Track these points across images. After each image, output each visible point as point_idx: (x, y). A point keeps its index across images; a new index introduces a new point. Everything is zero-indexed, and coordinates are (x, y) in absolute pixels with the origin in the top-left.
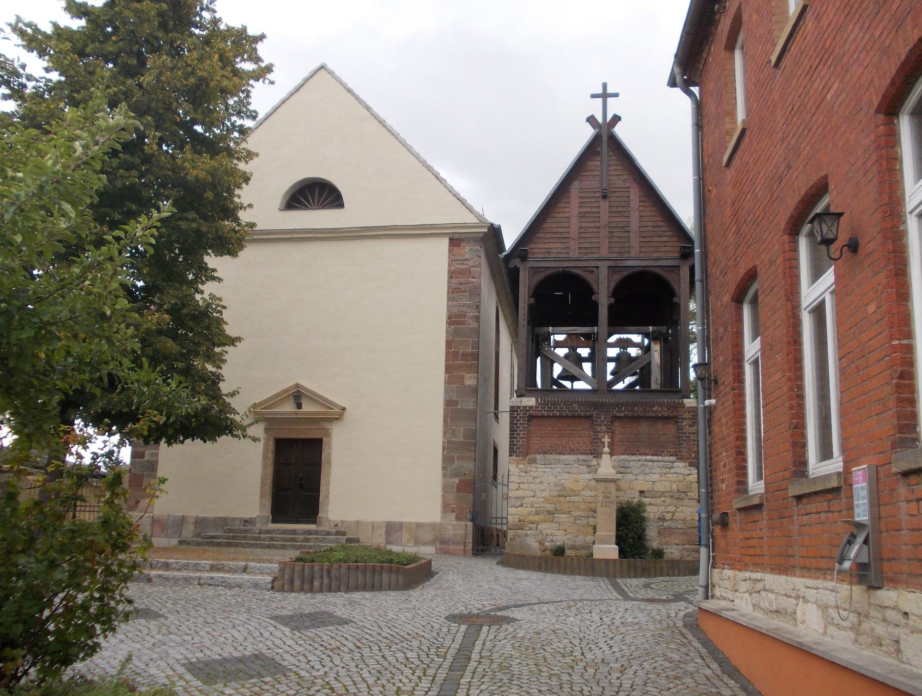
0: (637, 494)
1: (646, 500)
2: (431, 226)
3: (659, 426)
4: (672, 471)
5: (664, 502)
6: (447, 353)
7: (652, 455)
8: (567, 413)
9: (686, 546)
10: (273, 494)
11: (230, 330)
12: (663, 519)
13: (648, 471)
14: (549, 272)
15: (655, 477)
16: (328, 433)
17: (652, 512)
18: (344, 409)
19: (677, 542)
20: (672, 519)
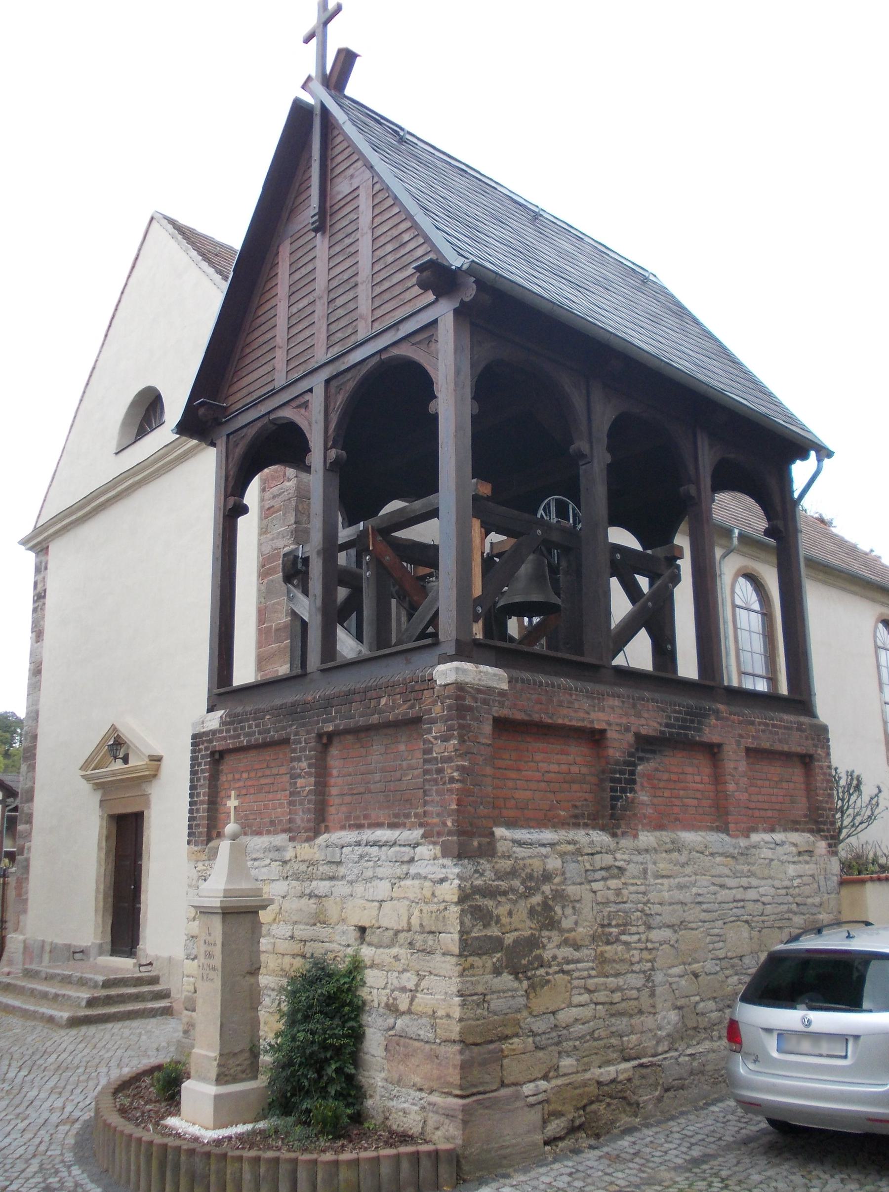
0: (353, 935)
1: (367, 953)
2: (271, 399)
3: (402, 747)
4: (413, 870)
5: (396, 958)
6: (260, 632)
7: (393, 826)
8: (258, 738)
9: (435, 1098)
10: (114, 905)
11: (868, 550)
12: (392, 1009)
13: (369, 873)
14: (251, 432)
15: (382, 889)
16: (146, 798)
17: (375, 987)
18: (158, 759)
19: (417, 1080)
20: (409, 1012)
